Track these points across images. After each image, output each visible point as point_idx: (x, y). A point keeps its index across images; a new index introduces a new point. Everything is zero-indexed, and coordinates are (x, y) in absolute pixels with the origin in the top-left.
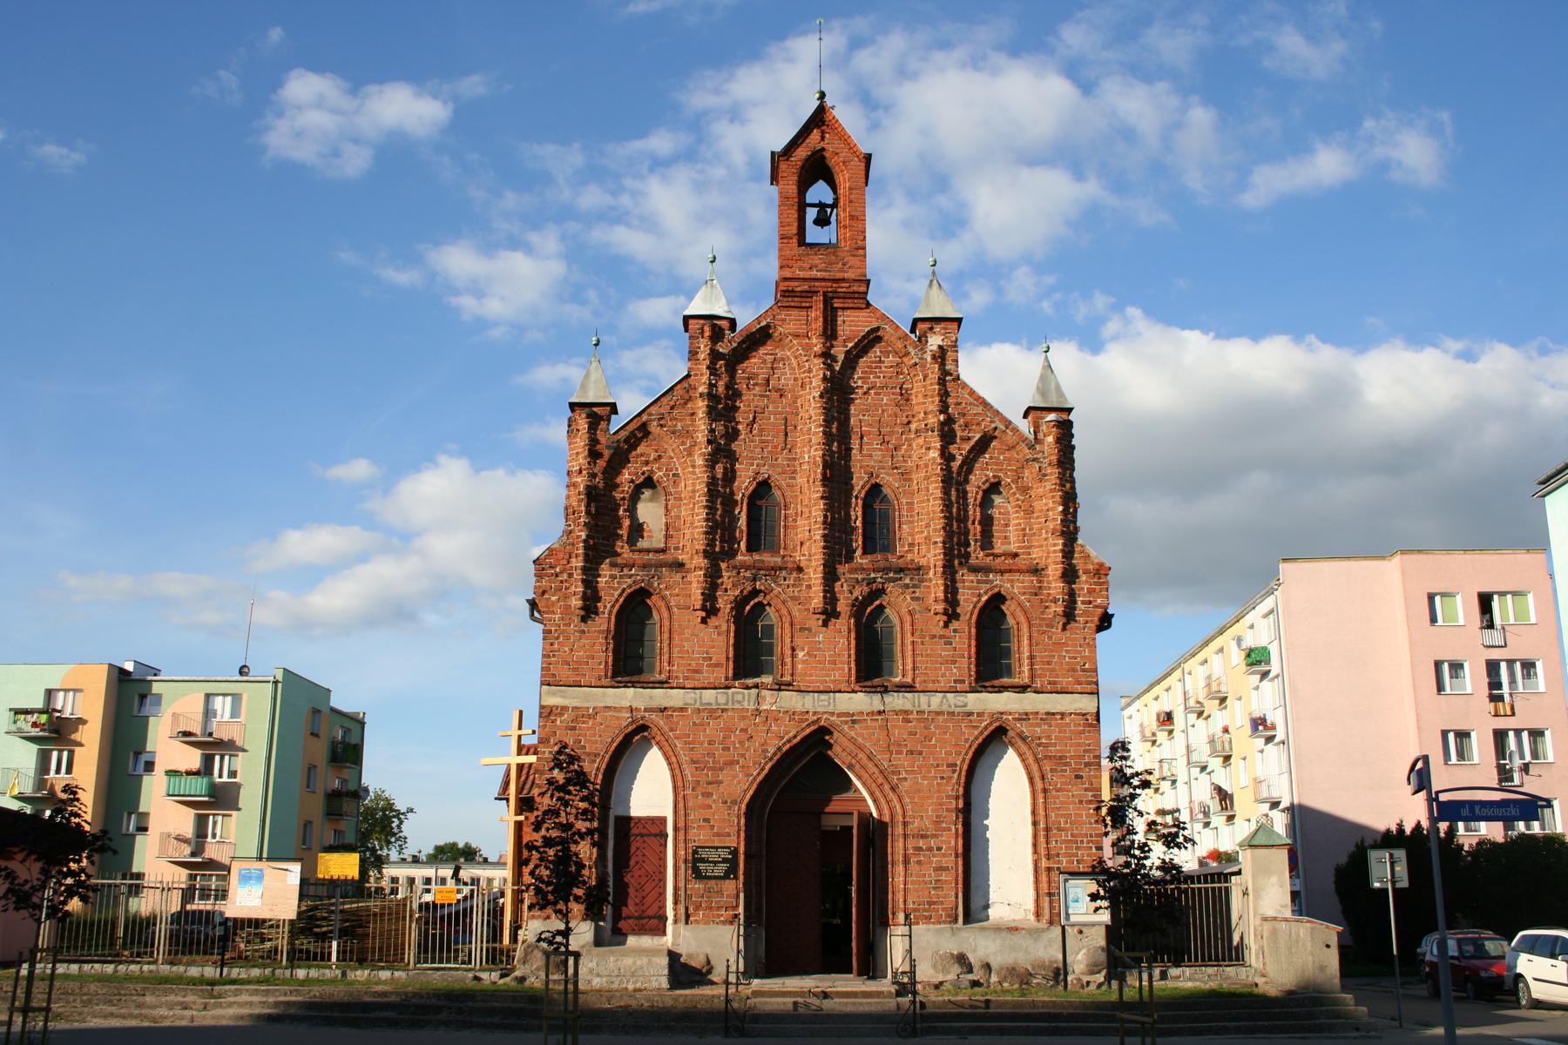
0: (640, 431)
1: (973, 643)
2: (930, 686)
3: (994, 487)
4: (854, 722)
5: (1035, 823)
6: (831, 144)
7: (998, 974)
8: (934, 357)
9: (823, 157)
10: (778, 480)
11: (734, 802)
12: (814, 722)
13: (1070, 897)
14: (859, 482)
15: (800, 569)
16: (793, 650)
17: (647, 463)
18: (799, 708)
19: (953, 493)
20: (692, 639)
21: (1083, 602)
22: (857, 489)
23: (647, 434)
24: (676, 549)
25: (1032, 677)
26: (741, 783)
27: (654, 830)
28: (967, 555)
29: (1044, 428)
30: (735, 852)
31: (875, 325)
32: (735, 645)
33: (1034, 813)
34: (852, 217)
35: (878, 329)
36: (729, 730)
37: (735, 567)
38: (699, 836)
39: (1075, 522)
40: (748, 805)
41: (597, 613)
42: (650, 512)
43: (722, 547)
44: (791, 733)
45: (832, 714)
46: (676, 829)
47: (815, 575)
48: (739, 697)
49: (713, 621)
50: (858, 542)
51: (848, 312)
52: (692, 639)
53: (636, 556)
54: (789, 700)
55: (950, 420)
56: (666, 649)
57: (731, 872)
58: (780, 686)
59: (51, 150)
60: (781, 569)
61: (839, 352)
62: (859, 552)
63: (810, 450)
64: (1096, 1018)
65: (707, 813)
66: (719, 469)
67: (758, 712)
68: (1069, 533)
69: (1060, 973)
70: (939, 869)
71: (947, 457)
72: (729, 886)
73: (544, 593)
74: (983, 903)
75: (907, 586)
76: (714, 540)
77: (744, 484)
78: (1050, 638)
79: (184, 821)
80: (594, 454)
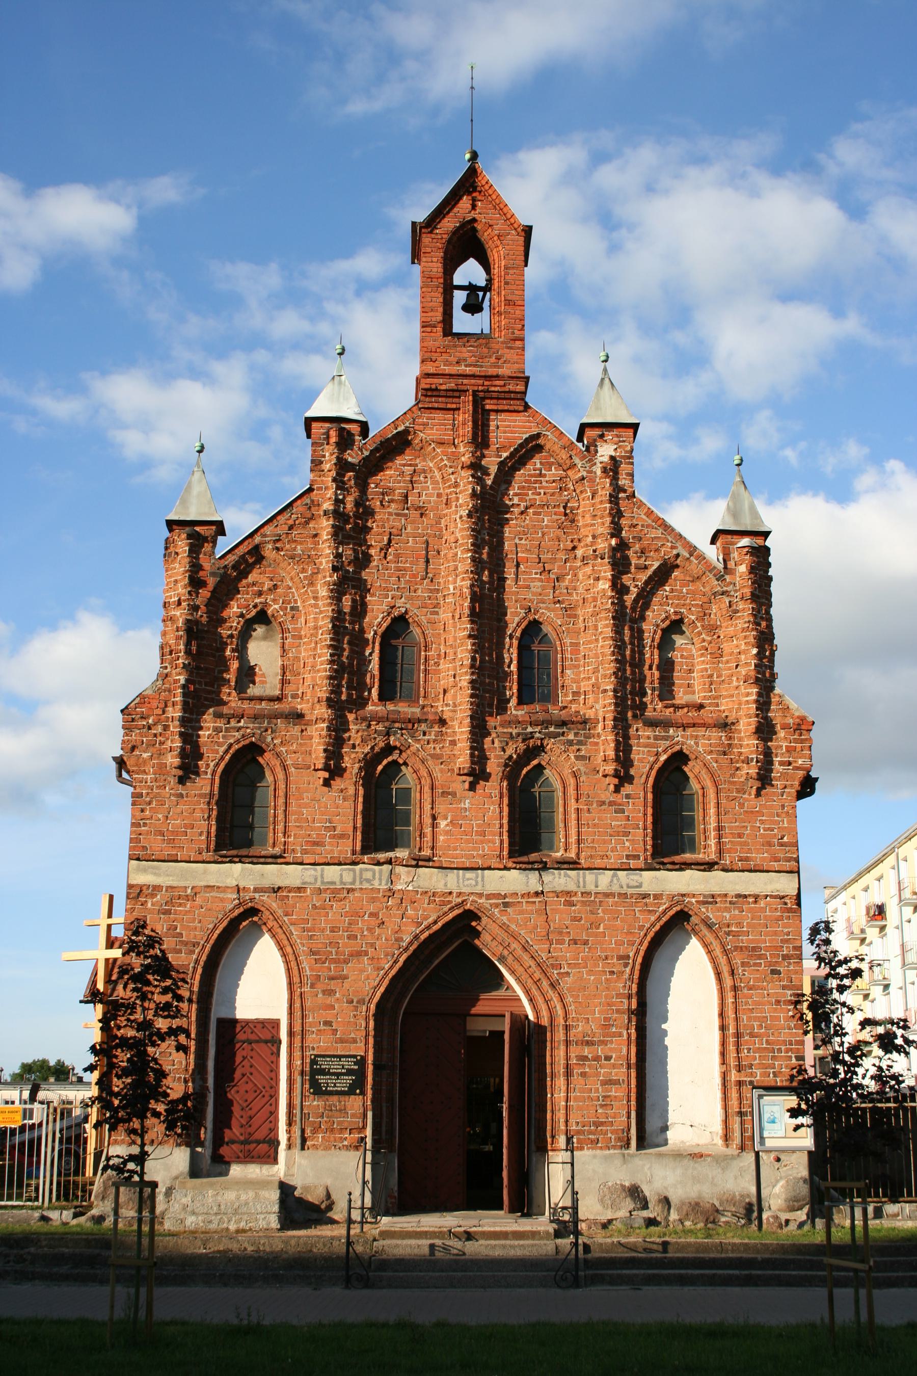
0: (251, 556)
1: (650, 811)
2: (598, 862)
3: (676, 626)
4: (506, 905)
5: (723, 1028)
6: (483, 215)
7: (679, 1210)
8: (604, 470)
9: (474, 230)
10: (417, 615)
11: (361, 1002)
12: (458, 905)
14: (514, 619)
15: (442, 722)
16: (434, 818)
17: (260, 594)
20: (313, 805)
21: (781, 763)
22: (511, 626)
23: (260, 559)
25: (720, 852)
26: (369, 979)
28: (643, 707)
29: (735, 555)
30: (362, 1062)
31: (535, 431)
34: (508, 303)
35: (538, 436)
36: (356, 914)
38: (319, 1043)
39: (772, 668)
40: (378, 1005)
41: (197, 774)
42: (263, 652)
43: (349, 695)
45: (480, 895)
46: (291, 1034)
47: (461, 729)
48: (369, 875)
49: (338, 783)
51: (503, 416)
53: (246, 705)
54: (429, 879)
56: (281, 817)
57: (357, 1087)
58: (418, 862)
60: (419, 721)
61: (492, 463)
62: (513, 702)
65: (328, 1015)
66: (347, 601)
67: (391, 893)
69: (753, 1210)
71: (619, 589)
72: (355, 1104)
73: (133, 748)
74: (660, 1125)
75: (570, 743)
76: (339, 686)
77: (376, 620)
78: (742, 805)
80: (195, 583)
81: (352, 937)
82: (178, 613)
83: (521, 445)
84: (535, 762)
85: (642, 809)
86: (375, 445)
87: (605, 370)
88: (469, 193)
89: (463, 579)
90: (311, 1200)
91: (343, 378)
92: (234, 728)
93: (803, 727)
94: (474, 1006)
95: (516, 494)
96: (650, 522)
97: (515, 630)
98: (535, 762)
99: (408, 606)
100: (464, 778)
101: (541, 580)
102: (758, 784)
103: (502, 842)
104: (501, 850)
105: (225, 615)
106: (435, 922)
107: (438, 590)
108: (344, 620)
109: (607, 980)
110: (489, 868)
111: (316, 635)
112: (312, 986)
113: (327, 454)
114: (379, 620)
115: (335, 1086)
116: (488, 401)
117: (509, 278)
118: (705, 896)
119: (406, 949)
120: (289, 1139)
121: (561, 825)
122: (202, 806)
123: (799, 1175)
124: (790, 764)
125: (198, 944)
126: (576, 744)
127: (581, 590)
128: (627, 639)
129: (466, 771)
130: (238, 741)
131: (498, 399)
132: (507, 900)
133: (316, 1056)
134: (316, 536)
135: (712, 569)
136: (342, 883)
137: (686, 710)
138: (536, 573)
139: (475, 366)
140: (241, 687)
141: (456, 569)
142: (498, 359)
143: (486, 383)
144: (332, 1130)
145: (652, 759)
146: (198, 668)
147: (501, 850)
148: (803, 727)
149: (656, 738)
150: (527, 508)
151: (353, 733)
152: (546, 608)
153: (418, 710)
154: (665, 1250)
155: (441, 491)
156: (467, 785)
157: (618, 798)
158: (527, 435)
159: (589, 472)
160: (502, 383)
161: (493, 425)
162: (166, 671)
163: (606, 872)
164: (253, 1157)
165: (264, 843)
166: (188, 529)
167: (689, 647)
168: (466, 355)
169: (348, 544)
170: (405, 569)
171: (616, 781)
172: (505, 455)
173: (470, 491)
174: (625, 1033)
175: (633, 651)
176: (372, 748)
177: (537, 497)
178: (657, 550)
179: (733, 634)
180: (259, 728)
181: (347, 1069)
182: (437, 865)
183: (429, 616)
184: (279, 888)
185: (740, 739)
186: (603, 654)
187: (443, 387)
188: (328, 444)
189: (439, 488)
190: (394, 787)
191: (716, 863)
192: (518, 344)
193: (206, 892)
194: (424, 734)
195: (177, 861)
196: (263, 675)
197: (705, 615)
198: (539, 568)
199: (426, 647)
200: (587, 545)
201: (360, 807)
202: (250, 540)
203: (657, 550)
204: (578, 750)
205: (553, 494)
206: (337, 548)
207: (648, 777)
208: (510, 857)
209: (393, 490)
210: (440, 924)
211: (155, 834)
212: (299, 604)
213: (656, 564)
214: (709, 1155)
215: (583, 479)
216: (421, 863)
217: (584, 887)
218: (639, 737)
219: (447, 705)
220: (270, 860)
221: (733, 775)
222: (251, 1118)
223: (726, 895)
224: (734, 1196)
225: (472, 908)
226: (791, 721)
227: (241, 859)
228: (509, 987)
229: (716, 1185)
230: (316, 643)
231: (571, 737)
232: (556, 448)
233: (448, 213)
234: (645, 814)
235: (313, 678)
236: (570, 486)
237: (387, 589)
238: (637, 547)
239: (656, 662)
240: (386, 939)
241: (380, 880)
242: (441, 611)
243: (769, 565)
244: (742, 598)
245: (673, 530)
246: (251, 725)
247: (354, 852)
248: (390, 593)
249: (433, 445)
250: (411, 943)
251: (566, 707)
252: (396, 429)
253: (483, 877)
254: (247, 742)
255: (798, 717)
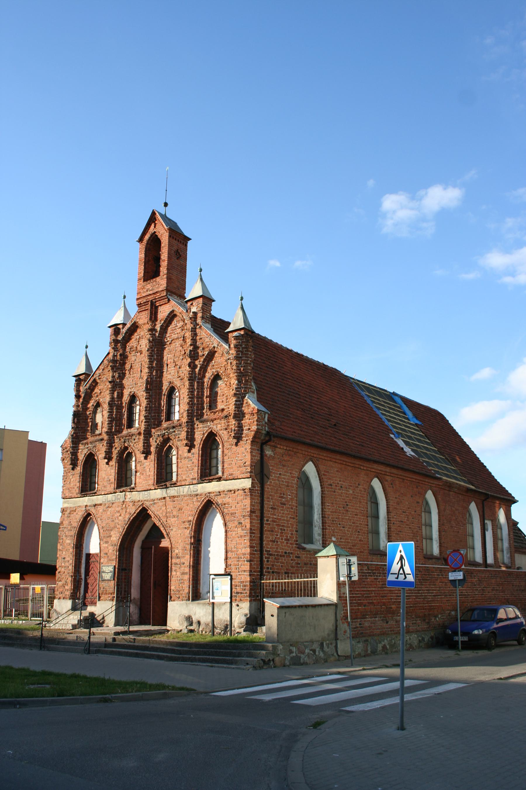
2: (183, 483)
3: (217, 377)
11: (115, 545)
13: (215, 588)
21: (246, 430)
22: (164, 390)
28: (202, 415)
31: (171, 310)
35: (173, 311)
41: (77, 466)
43: (115, 429)
44: (133, 510)
45: (147, 501)
59: (298, 263)
64: (173, 651)
70: (183, 574)
71: (192, 366)
76: (112, 426)
84: (168, 445)
98: (168, 445)
105: (88, 406)
108: (115, 401)
146: (77, 427)
154: (134, 642)
157: (190, 454)
175: (198, 392)
194: (134, 440)
213: (207, 353)
223: (224, 491)
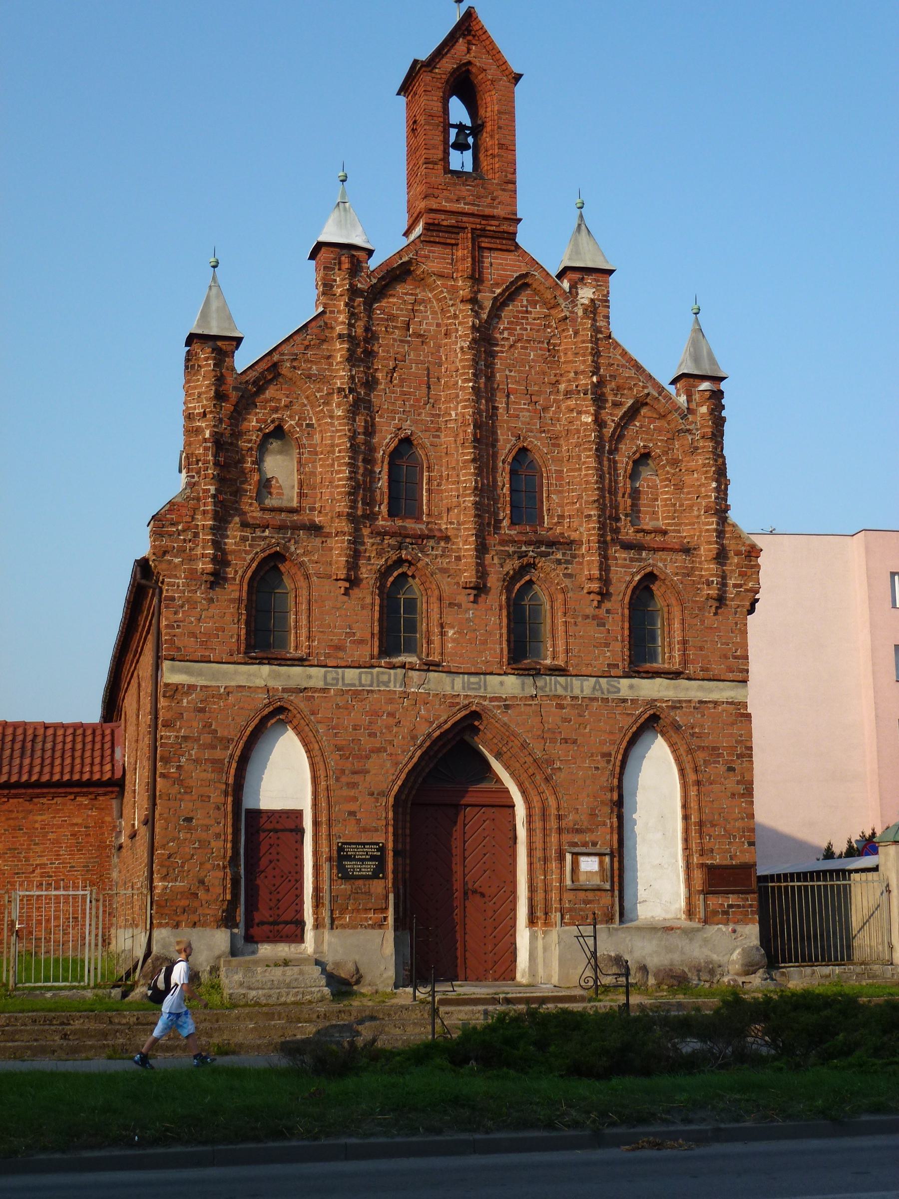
0: (270, 370)
1: (627, 625)
2: (584, 670)
3: (644, 458)
4: (507, 707)
5: (686, 818)
6: (478, 58)
7: (656, 975)
8: (585, 311)
9: (468, 71)
10: (423, 438)
11: (382, 794)
12: (466, 707)
14: (506, 445)
15: (447, 539)
16: (442, 626)
17: (276, 410)
18: (448, 691)
19: (606, 463)
20: (327, 607)
24: (312, 509)
25: (685, 661)
26: (387, 773)
27: (290, 825)
28: (617, 531)
29: (697, 397)
30: (382, 849)
32: (381, 620)
33: (685, 806)
34: (501, 146)
35: (526, 275)
36: (376, 714)
37: (379, 534)
38: (348, 832)
39: (726, 500)
40: (396, 797)
42: (279, 467)
45: (484, 698)
46: (316, 823)
47: (466, 546)
48: (385, 678)
49: (356, 593)
50: (505, 515)
51: (495, 254)
52: (327, 607)
53: (267, 516)
54: (439, 682)
55: (601, 384)
56: (304, 622)
57: (378, 873)
58: (430, 666)
60: (429, 537)
61: (487, 299)
62: (505, 523)
63: (458, 410)
65: (352, 807)
66: (360, 421)
67: (406, 695)
68: (721, 511)
71: (599, 423)
72: (377, 887)
73: (165, 553)
75: (559, 562)
76: (354, 501)
77: (385, 440)
78: (702, 622)
79: (538, 798)
80: (220, 397)
81: (372, 735)
82: (204, 425)
83: (512, 283)
84: (527, 578)
85: (620, 623)
86: (382, 273)
87: (581, 216)
88: (464, 36)
89: (465, 407)
90: (343, 975)
91: (347, 205)
92: (260, 537)
93: (753, 554)
94: (464, 797)
95: (505, 329)
96: (624, 362)
97: (507, 455)
98: (527, 578)
99: (413, 428)
100: (469, 591)
101: (528, 410)
102: (715, 604)
103: (502, 650)
104: (502, 657)
106: (446, 722)
107: (439, 415)
109: (593, 775)
110: (491, 674)
111: (333, 452)
112: (337, 779)
113: (338, 279)
114: (387, 440)
115: (360, 871)
116: (483, 239)
117: (502, 122)
118: (673, 701)
119: (420, 746)
120: (316, 920)
121: (549, 635)
122: (232, 610)
123: (752, 945)
124: (741, 586)
125: (233, 740)
126: (564, 563)
127: (564, 422)
128: (605, 469)
129: (472, 585)
130: (263, 551)
131: (492, 237)
132: (507, 703)
133: (343, 843)
134: (329, 357)
135: (678, 408)
136: (361, 685)
137: (653, 535)
138: (525, 404)
139: (473, 204)
140: (259, 498)
141: (457, 396)
142: (493, 199)
143: (483, 222)
144: (358, 910)
145: (628, 579)
147: (502, 657)
148: (753, 554)
149: (632, 560)
150: (516, 342)
151: (368, 547)
152: (534, 437)
153: (424, 527)
155: (440, 321)
156: (472, 598)
158: (518, 274)
159: (572, 312)
160: (497, 223)
161: (487, 261)
162: (193, 480)
163: (590, 679)
164: (282, 937)
165: (537, 653)
166: (210, 343)
167: (654, 477)
168: (465, 193)
169: (359, 366)
170: (409, 393)
171: (599, 598)
172: (498, 291)
173: (471, 324)
174: (608, 821)
175: (610, 480)
176: (386, 560)
177: (524, 332)
178: (630, 389)
179: (694, 468)
180: (284, 538)
181: (371, 856)
182: (446, 669)
183: (431, 439)
184: (305, 688)
185: (700, 563)
186: (587, 482)
187: (445, 223)
188: (339, 269)
189: (443, 320)
190: (402, 597)
191: (682, 673)
192: (510, 186)
193: (238, 692)
195: (210, 662)
196: (280, 487)
197: (669, 449)
198: (526, 400)
199: (429, 468)
200: (569, 381)
201: (377, 615)
202: (269, 358)
203: (630, 389)
204: (566, 568)
205: (538, 331)
206: (351, 370)
207: (624, 595)
208: (509, 664)
209: (398, 316)
210: (449, 724)
211: (188, 636)
212: (314, 422)
214: (679, 928)
215: (566, 318)
216: (431, 668)
217: (572, 691)
218: (616, 559)
219: (451, 523)
220: (296, 663)
221: (696, 595)
222: (279, 901)
223: (690, 701)
224: (700, 963)
225: (478, 709)
226: (743, 548)
227: (270, 661)
228: (499, 780)
229: (684, 953)
230: (333, 460)
231: (559, 556)
232: (542, 288)
233: (446, 54)
234: (623, 628)
235: (331, 493)
236: (553, 324)
237: (395, 412)
238: (613, 385)
239: (628, 491)
240: (403, 737)
241: (395, 683)
242: (442, 435)
243: (723, 407)
244: (703, 437)
245: (644, 371)
246: (276, 535)
247: (372, 657)
248: (397, 416)
249: (434, 278)
250: (424, 741)
251: (551, 529)
252: (401, 259)
253: (485, 681)
254: (273, 551)
255: (749, 545)
